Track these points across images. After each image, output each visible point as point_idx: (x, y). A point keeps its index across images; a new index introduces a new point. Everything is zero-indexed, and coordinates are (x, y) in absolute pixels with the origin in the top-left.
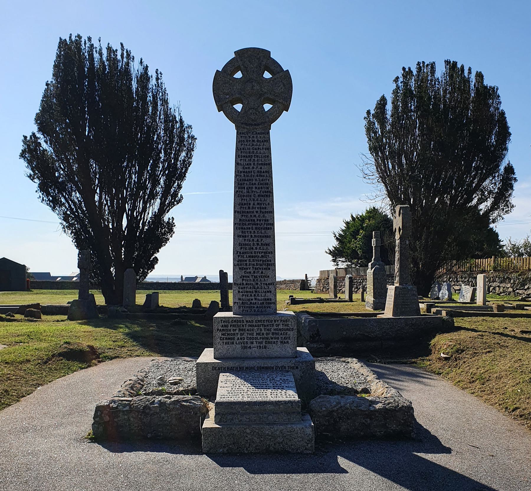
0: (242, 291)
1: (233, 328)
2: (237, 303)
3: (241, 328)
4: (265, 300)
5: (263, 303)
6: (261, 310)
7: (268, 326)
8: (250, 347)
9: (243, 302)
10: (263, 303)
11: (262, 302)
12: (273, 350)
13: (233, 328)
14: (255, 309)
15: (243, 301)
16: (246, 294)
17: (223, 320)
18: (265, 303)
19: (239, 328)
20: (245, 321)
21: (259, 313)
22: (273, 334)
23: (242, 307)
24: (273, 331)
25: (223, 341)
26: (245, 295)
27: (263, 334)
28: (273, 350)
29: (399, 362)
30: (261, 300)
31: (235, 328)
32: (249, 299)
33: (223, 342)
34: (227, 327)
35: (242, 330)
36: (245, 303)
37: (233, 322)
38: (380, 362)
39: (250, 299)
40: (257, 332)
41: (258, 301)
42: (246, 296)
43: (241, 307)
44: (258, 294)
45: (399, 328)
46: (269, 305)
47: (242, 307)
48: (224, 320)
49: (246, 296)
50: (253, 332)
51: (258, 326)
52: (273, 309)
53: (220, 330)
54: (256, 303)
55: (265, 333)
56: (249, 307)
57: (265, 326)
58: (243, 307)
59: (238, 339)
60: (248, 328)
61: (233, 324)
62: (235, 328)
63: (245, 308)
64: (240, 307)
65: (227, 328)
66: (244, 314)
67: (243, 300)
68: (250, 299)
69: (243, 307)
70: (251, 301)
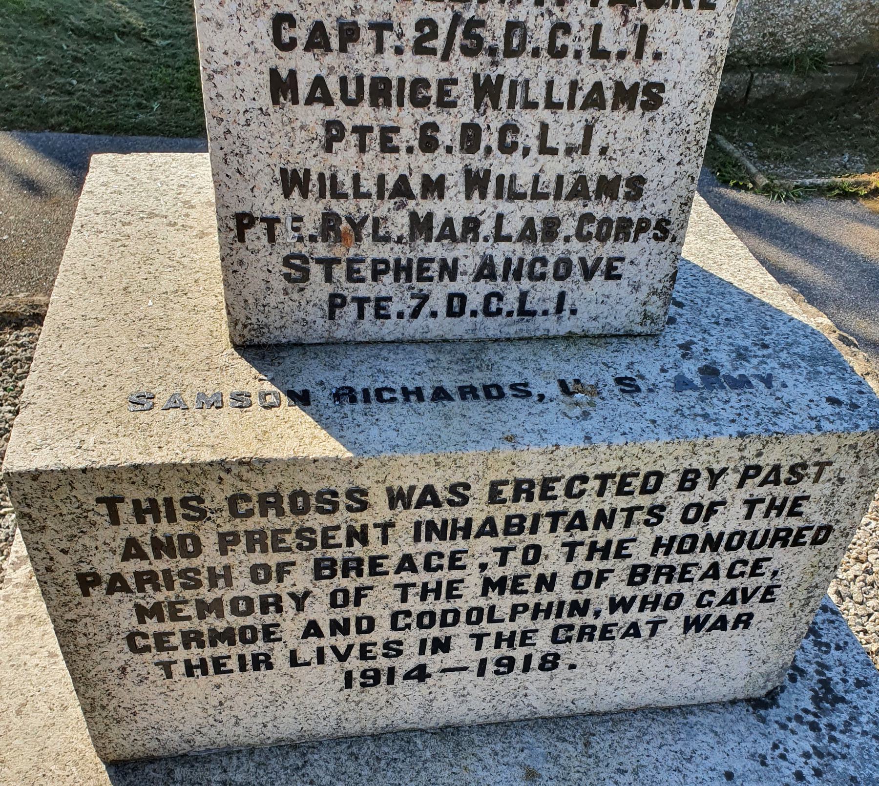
0: (319, 82)
1: (258, 558)
2: (271, 222)
3: (338, 554)
4: (580, 191)
5: (551, 226)
6: (523, 296)
7: (604, 519)
8: (420, 674)
9: (329, 220)
10: (551, 226)
11: (540, 210)
12: (611, 675)
13: (258, 558)
14: (460, 285)
15: (340, 208)
16: (364, 114)
17: (131, 493)
18: (568, 227)
19: (318, 552)
20: (378, 499)
21: (492, 327)
22: (638, 575)
23: (328, 264)
24: (640, 554)
25: (164, 656)
26: (362, 131)
27: (546, 583)
28: (611, 675)
29: (831, 188)
30: (537, 196)
31: (273, 559)
32: (402, 189)
33: (167, 667)
34: (187, 555)
35: (353, 566)
36: (357, 226)
37: (243, 507)
38: (767, 190)
39: (415, 184)
40: (495, 573)
41: (504, 206)
42: (374, 140)
43: (316, 271)
44: (510, 128)
45: (822, 19)
46: (609, 249)
47: (328, 264)
48: (143, 494)
49: (374, 140)
50: (456, 574)
51: (515, 525)
52: (636, 288)
53: (116, 583)
54: (472, 225)
55: (566, 571)
56: (402, 270)
57: (579, 521)
58: (339, 272)
59: (312, 629)
60: (410, 549)
61: (255, 522)
62: (273, 559)
63: (352, 275)
64: (305, 275)
65: (184, 563)
66: (341, 333)
67: (338, 195)
68: (415, 184)
69: (339, 272)
70: (423, 207)
